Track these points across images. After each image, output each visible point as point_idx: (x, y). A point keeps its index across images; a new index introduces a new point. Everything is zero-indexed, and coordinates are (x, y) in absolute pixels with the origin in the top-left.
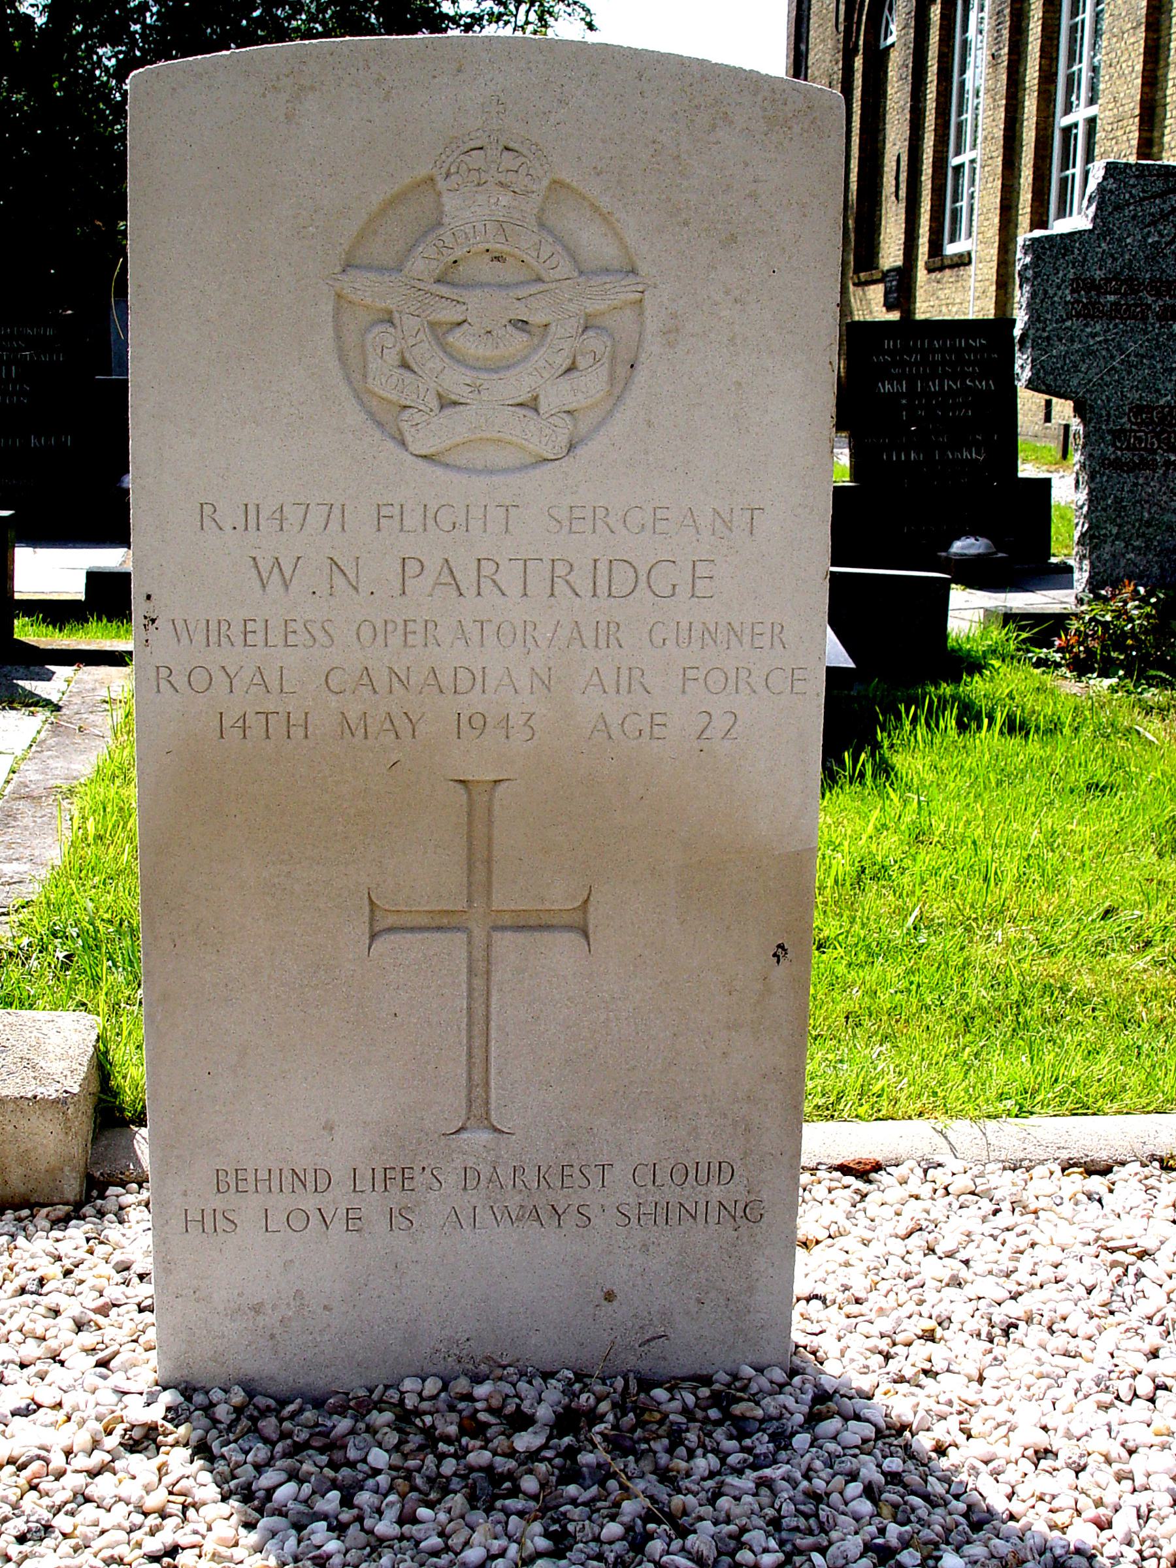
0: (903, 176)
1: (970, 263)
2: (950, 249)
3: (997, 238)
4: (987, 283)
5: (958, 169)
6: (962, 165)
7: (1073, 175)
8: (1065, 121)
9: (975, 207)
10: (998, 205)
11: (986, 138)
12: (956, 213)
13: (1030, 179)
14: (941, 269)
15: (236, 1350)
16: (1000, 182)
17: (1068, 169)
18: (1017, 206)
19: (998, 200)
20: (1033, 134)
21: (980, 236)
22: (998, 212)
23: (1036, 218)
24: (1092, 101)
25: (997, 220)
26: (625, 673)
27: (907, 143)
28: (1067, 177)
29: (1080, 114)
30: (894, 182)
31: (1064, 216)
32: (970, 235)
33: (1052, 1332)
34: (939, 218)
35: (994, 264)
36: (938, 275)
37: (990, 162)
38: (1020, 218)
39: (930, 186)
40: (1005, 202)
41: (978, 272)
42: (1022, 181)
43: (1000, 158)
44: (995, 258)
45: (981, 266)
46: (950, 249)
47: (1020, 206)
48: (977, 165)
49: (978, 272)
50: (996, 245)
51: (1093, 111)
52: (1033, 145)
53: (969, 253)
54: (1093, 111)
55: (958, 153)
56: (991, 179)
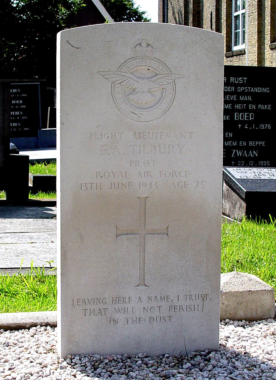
0: (214, 20)
1: (245, 53)
2: (235, 48)
3: (257, 44)
4: (254, 62)
5: (237, 17)
6: (239, 15)
7: (239, 32)
8: (235, 14)
9: (246, 31)
10: (257, 31)
11: (250, 5)
12: (236, 34)
13: (269, 21)
14: (232, 56)
15: (87, 344)
16: (257, 22)
17: (237, 30)
18: (264, 31)
19: (256, 29)
20: (270, 3)
21: (250, 43)
22: (257, 33)
23: (273, 35)
24: (244, 8)
25: (256, 37)
26: (146, 173)
27: (215, 7)
28: (237, 32)
29: (240, 12)
30: (210, 23)
31: (237, 45)
32: (244, 42)
33: (260, 346)
34: (229, 36)
35: (256, 54)
36: (231, 59)
37: (252, 14)
38: (266, 36)
39: (225, 24)
40: (259, 30)
41: (249, 57)
42: (266, 21)
43: (257, 13)
44: (256, 52)
45: (250, 55)
46: (235, 48)
47: (266, 31)
48: (247, 16)
49: (249, 57)
50: (257, 46)
51: (244, 11)
52: (270, 7)
53: (244, 50)
54: (244, 11)
55: (236, 11)
56: (253, 21)
